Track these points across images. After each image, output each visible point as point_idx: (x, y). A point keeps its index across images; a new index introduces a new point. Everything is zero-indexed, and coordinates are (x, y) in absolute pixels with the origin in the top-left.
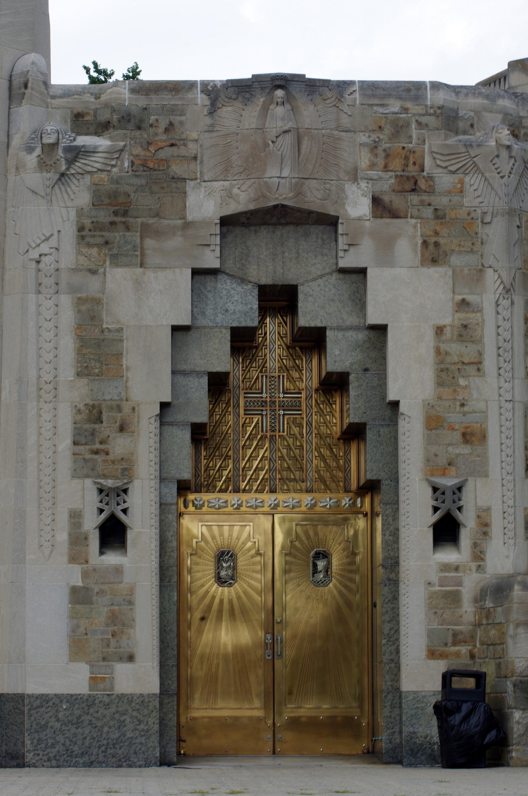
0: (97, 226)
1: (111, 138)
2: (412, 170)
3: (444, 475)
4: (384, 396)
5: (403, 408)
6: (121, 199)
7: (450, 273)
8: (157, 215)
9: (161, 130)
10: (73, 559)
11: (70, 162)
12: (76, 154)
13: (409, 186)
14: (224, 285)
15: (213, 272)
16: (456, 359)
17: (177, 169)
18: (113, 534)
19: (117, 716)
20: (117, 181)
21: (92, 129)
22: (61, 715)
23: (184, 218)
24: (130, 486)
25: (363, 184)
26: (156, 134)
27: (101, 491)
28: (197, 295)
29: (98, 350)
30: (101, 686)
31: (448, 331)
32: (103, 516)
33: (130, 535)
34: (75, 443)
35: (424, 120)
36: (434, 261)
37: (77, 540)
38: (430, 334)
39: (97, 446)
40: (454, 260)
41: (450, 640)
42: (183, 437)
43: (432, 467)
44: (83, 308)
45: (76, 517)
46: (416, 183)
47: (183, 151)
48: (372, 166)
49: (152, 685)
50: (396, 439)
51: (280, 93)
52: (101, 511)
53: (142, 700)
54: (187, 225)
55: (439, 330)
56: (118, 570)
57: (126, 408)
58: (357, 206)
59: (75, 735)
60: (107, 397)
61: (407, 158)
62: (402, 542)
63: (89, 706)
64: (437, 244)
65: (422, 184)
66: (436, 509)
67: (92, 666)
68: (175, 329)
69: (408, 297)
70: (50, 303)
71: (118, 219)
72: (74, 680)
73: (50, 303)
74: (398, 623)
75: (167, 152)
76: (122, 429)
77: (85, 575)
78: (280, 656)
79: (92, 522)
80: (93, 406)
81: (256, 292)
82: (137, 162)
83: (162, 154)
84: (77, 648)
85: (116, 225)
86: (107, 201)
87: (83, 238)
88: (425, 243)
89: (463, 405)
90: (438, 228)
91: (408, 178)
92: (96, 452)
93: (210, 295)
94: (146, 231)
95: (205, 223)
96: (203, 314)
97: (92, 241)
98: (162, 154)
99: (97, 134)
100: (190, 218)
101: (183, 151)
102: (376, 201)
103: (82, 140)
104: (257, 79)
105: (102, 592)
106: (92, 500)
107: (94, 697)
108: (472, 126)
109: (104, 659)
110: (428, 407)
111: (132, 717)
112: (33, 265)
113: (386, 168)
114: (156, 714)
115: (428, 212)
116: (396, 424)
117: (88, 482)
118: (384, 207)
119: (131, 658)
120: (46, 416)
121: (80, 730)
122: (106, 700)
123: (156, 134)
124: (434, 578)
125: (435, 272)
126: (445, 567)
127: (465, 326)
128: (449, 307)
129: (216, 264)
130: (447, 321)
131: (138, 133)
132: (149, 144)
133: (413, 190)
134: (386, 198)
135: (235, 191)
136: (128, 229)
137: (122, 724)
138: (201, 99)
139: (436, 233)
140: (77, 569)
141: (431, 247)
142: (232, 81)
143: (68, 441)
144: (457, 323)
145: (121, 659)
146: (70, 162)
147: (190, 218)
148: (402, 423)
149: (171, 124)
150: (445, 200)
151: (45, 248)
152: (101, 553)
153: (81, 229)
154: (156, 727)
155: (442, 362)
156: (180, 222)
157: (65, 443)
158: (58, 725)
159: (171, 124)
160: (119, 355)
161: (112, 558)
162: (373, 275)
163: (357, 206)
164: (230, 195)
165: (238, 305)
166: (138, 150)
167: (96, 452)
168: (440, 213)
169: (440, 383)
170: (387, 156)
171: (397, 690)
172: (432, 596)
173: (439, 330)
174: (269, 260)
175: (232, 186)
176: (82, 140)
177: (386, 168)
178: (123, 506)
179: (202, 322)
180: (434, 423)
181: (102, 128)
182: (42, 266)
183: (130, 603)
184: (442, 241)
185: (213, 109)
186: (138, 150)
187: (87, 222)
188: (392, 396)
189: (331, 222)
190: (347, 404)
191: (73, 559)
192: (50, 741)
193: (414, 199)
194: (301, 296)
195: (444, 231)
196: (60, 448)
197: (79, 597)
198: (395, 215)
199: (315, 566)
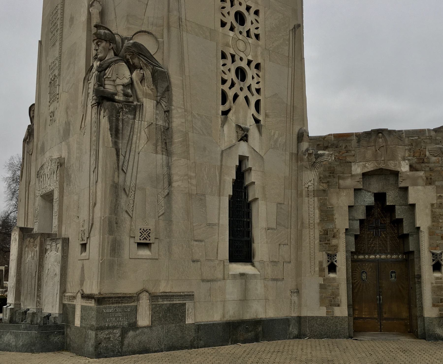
0: (325, 177)
1: (328, 151)
2: (422, 156)
3: (435, 249)
4: (415, 226)
5: (421, 229)
6: (332, 169)
7: (435, 187)
8: (343, 173)
9: (343, 148)
10: (320, 276)
11: (316, 159)
12: (318, 156)
13: (421, 161)
14: (363, 193)
15: (360, 190)
16: (438, 214)
17: (348, 159)
18: (332, 268)
19: (335, 323)
20: (330, 163)
21: (322, 148)
22: (318, 322)
23: (351, 174)
24: (337, 254)
25: (407, 161)
26: (342, 149)
27: (328, 255)
28: (355, 196)
29: (327, 214)
30: (330, 314)
31: (435, 205)
32: (329, 263)
33: (337, 269)
34: (320, 241)
35: (426, 141)
36: (430, 184)
37: (321, 270)
38: (429, 206)
39: (327, 242)
40: (437, 183)
41: (440, 301)
42: (352, 239)
43: (431, 246)
44: (321, 201)
45: (321, 263)
46: (423, 160)
47: (350, 154)
48: (409, 156)
49: (346, 314)
50: (419, 238)
51: (380, 135)
52: (328, 261)
53: (343, 318)
54: (352, 176)
55: (432, 205)
56: (334, 279)
57: (335, 231)
58: (404, 168)
59: (322, 329)
60: (329, 227)
61: (420, 153)
62: (422, 270)
63: (326, 320)
64: (431, 179)
65: (425, 160)
66: (433, 260)
67: (327, 308)
68: (349, 207)
69: (421, 196)
70: (312, 200)
71: (331, 175)
72: (322, 312)
73: (312, 200)
74: (422, 295)
75: (346, 154)
76: (334, 237)
77: (324, 280)
78: (292, 154)
79: (325, 265)
80: (325, 230)
81: (373, 195)
82: (337, 158)
83: (344, 155)
84: (322, 301)
85: (331, 177)
86: (328, 169)
87: (321, 180)
88: (427, 178)
89: (441, 228)
90: (431, 174)
91: (421, 159)
92: (326, 244)
93: (359, 196)
94: (339, 178)
95: (357, 175)
96: (357, 202)
97: (323, 181)
98: (344, 155)
99: (324, 150)
100: (353, 173)
101: (350, 154)
102: (411, 166)
103: (320, 152)
104: (372, 131)
105: (329, 286)
106: (325, 257)
107: (328, 317)
108: (441, 142)
109: (330, 306)
110: (429, 228)
111: (339, 323)
112: (306, 189)
113: (414, 156)
114: (347, 323)
115: (428, 169)
116: (419, 234)
117: (324, 252)
118: (414, 168)
119: (339, 306)
120: (311, 233)
121: (324, 327)
122: (332, 318)
123: (342, 149)
124: (434, 282)
125: (429, 187)
126: (437, 278)
127: (441, 204)
128: (435, 198)
129: (361, 187)
130: (435, 202)
131: (336, 149)
132: (340, 152)
133: (423, 162)
134: (414, 165)
135: (367, 165)
136: (334, 177)
137: (336, 326)
138: (354, 138)
139: (431, 175)
140: (322, 279)
141: (429, 180)
142: (365, 132)
143: (318, 241)
144: (438, 203)
145: (336, 306)
146: (316, 159)
147: (353, 173)
148: (420, 233)
149: (346, 146)
150: (433, 165)
151: (310, 184)
152: (329, 274)
153: (320, 178)
154: (347, 327)
155: (433, 215)
156: (350, 175)
157: (317, 241)
158: (317, 326)
159: (346, 146)
160: (333, 215)
161: (332, 275)
162: (411, 190)
163: (404, 168)
164: (365, 166)
165: (369, 200)
166: (337, 154)
167: (326, 244)
168: (432, 169)
169: (433, 221)
170: (414, 152)
171: (422, 316)
172: (433, 287)
173: (432, 205)
174: (376, 186)
175: (366, 164)
176: (320, 152)
177: (414, 156)
178: (336, 260)
179: (357, 204)
180: (431, 233)
181: (326, 148)
182: (309, 189)
183: (338, 289)
184: (433, 178)
185: (359, 141)
186: (337, 154)
187: (322, 176)
188: (418, 226)
189: (396, 174)
190: (83, 231)
191: (320, 276)
192: (315, 331)
193: (423, 165)
194: (387, 196)
195: (433, 174)
196: (316, 243)
197: (322, 287)
198: (417, 170)
199: (391, 275)
